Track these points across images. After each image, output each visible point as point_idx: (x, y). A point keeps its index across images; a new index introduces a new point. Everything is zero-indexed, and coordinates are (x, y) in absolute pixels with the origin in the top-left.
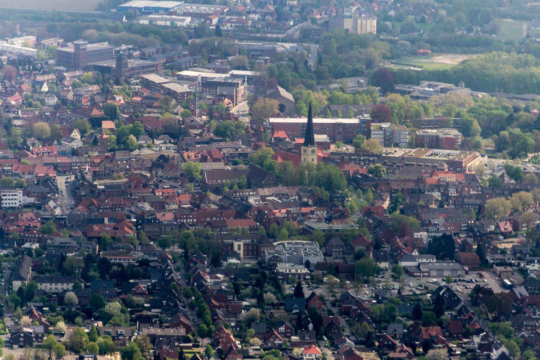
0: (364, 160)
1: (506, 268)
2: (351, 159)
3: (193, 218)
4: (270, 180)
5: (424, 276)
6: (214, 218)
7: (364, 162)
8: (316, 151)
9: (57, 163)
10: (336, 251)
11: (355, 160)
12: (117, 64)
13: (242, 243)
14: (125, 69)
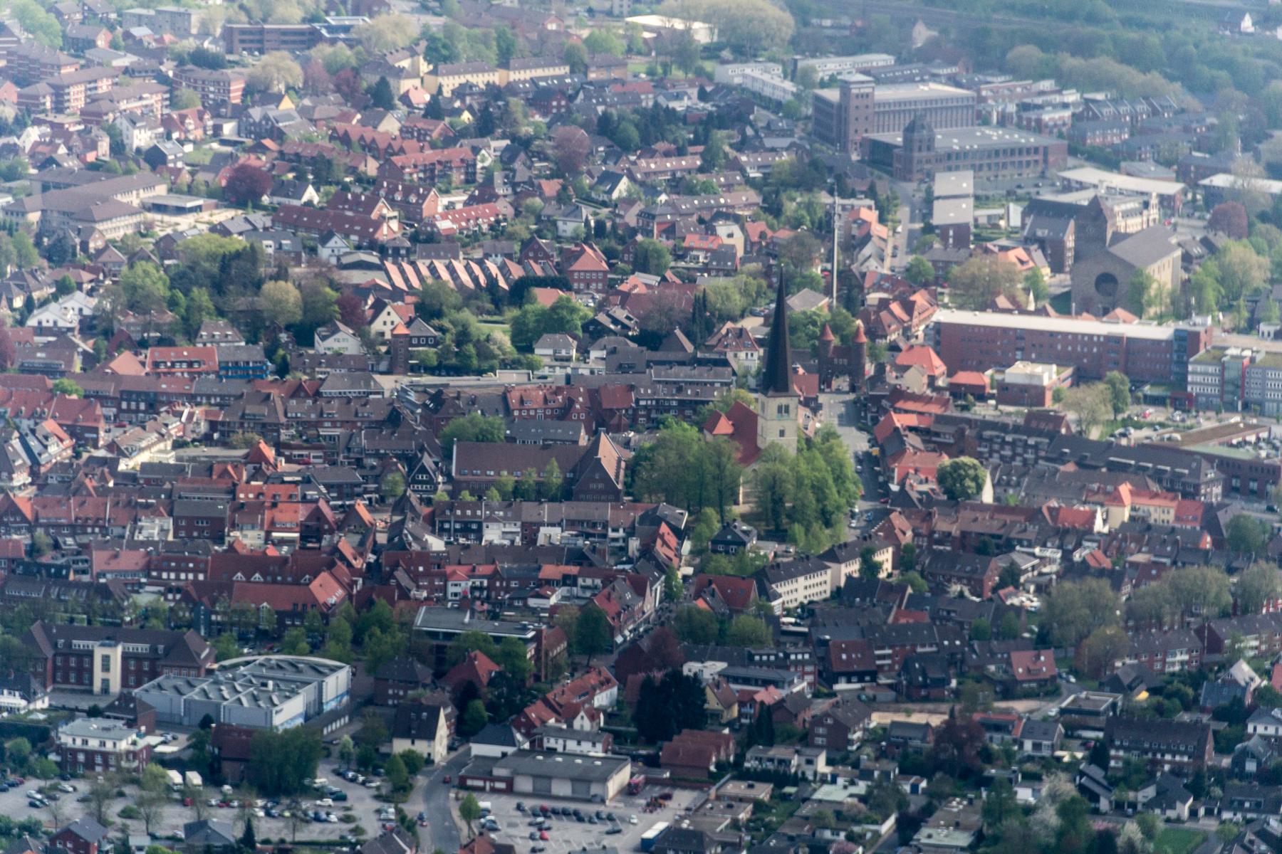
0: (1013, 444)
1: (751, 786)
6: (257, 575)
7: (1013, 450)
8: (791, 409)
9: (156, 394)
12: (905, 139)
13: (116, 654)
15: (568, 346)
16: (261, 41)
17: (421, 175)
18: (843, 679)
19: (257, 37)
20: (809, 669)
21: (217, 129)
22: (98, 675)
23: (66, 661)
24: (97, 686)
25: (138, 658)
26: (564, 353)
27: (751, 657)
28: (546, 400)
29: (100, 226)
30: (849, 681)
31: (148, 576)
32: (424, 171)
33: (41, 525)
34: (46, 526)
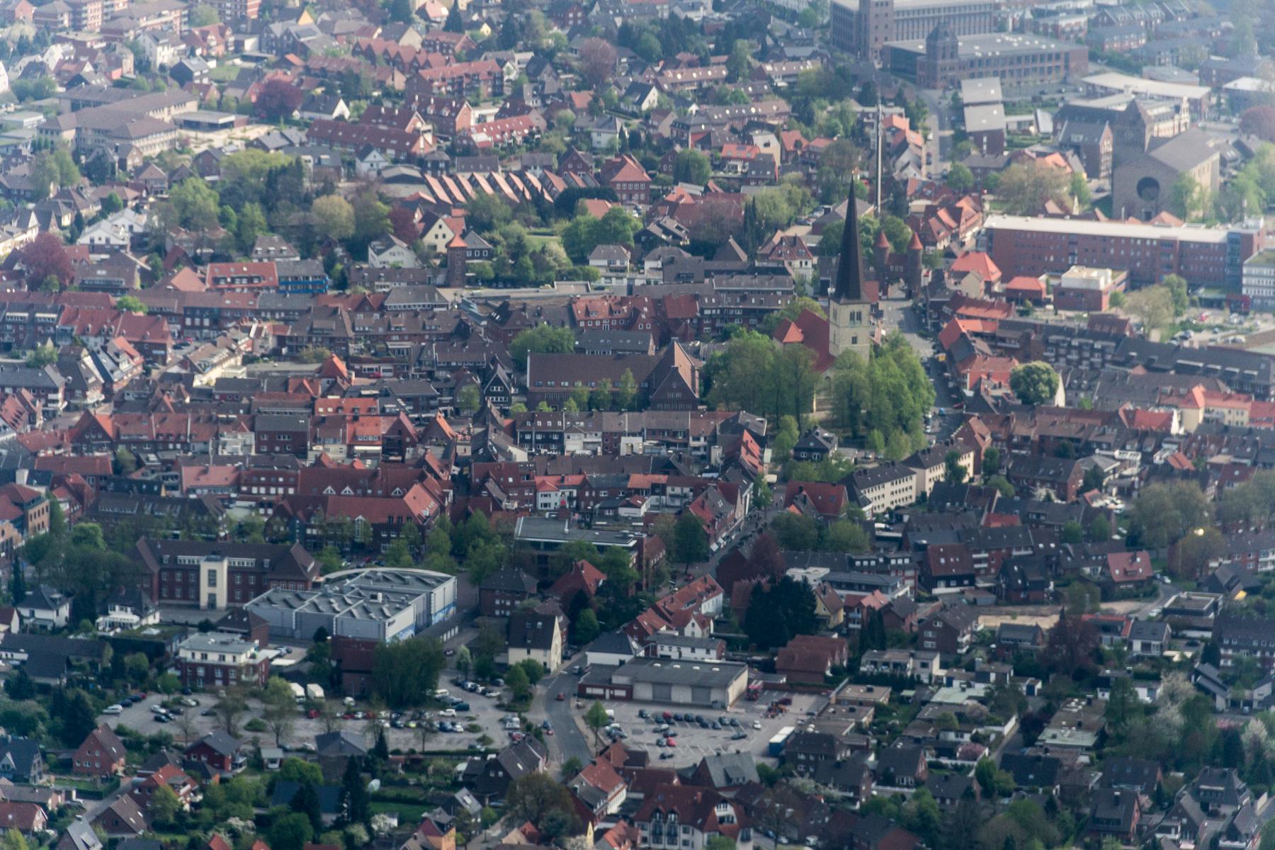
0: (1080, 348)
1: (870, 690)
2: (1046, 342)
3: (285, 485)
4: (672, 390)
5: (613, 698)
6: (347, 488)
7: (1080, 354)
9: (220, 310)
10: (503, 607)
11: (1057, 345)
12: (929, 46)
14: (948, 61)
17: (449, 88)
18: (942, 583)
21: (239, 45)
22: (205, 590)
23: (172, 576)
24: (204, 601)
26: (618, 263)
27: (852, 562)
28: (611, 311)
30: (948, 586)
31: (238, 491)
32: (452, 85)
33: (123, 442)
34: (128, 443)
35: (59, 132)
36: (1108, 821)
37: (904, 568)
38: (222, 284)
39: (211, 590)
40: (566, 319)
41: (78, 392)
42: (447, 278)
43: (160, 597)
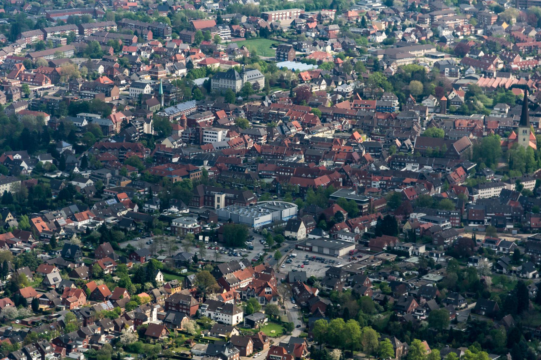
1: (388, 255)
15: (505, 108)
16: (526, 4)
17: (526, 50)
18: (473, 223)
19: (525, 3)
20: (457, 218)
21: (476, 32)
22: (216, 204)
23: (208, 198)
24: (216, 206)
25: (230, 199)
26: (503, 110)
27: (438, 213)
28: (468, 125)
29: (397, 61)
30: (474, 224)
31: (275, 173)
32: (528, 49)
33: (263, 155)
34: (265, 155)
35: (377, 55)
36: (401, 306)
37: (455, 216)
38: (357, 107)
39: (218, 204)
40: (452, 126)
41: (271, 138)
42: (440, 110)
43: (205, 204)
